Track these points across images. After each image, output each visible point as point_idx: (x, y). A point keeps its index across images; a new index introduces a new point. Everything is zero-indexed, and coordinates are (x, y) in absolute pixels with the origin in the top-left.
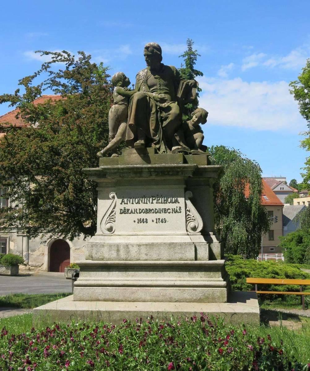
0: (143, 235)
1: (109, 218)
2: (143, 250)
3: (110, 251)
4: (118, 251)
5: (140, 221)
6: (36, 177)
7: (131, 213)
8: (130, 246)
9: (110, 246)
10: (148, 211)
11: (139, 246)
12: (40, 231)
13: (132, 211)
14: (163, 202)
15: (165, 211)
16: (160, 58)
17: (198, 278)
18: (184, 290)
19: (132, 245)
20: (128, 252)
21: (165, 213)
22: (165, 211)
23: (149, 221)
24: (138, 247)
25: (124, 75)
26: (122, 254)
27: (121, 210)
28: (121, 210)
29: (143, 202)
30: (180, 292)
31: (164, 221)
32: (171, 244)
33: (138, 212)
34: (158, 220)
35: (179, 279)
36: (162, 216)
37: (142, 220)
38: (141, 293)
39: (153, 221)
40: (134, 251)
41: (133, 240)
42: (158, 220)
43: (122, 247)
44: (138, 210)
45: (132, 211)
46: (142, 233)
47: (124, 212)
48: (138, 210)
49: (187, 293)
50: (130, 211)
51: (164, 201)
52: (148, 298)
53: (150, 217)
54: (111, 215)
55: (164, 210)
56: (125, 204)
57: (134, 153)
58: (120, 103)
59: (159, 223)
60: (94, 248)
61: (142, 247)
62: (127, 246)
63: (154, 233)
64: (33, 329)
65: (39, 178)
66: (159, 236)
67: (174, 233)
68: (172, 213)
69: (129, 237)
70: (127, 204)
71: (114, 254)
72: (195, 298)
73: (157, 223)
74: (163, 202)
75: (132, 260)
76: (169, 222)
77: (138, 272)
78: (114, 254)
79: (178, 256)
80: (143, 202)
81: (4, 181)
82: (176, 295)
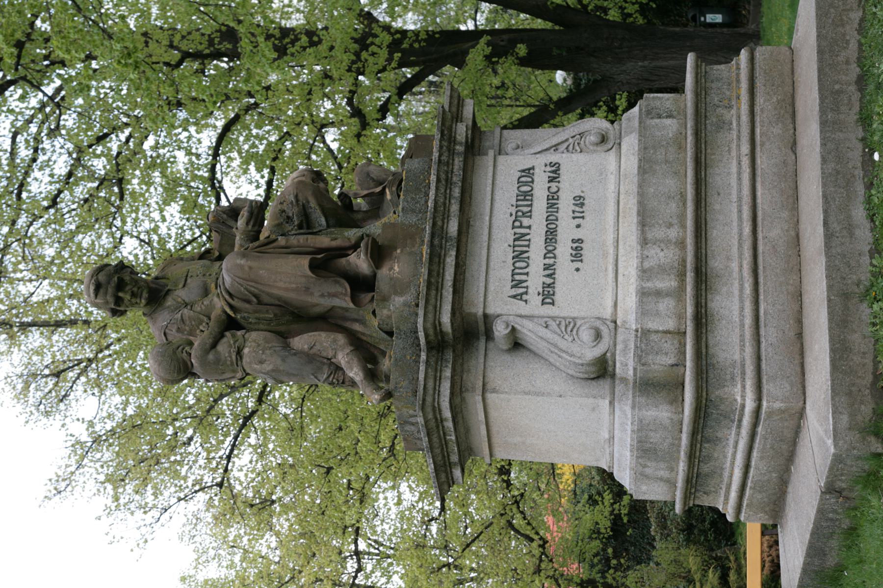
2: (657, 233)
4: (658, 294)
5: (577, 255)
7: (554, 279)
8: (646, 265)
10: (551, 236)
12: (381, 548)
14: (529, 203)
15: (553, 200)
19: (643, 259)
21: (557, 199)
22: (553, 200)
23: (578, 233)
26: (668, 283)
30: (767, 144)
31: (579, 201)
33: (551, 261)
35: (734, 146)
36: (566, 205)
39: (578, 226)
42: (579, 215)
43: (649, 285)
44: (547, 261)
46: (611, 250)
48: (547, 261)
51: (527, 200)
56: (526, 293)
59: (583, 212)
61: (649, 236)
62: (645, 273)
66: (621, 211)
67: (613, 177)
68: (559, 182)
69: (620, 278)
70: (527, 287)
71: (666, 305)
73: (583, 217)
74: (529, 203)
75: (684, 261)
76: (584, 189)
78: (666, 305)
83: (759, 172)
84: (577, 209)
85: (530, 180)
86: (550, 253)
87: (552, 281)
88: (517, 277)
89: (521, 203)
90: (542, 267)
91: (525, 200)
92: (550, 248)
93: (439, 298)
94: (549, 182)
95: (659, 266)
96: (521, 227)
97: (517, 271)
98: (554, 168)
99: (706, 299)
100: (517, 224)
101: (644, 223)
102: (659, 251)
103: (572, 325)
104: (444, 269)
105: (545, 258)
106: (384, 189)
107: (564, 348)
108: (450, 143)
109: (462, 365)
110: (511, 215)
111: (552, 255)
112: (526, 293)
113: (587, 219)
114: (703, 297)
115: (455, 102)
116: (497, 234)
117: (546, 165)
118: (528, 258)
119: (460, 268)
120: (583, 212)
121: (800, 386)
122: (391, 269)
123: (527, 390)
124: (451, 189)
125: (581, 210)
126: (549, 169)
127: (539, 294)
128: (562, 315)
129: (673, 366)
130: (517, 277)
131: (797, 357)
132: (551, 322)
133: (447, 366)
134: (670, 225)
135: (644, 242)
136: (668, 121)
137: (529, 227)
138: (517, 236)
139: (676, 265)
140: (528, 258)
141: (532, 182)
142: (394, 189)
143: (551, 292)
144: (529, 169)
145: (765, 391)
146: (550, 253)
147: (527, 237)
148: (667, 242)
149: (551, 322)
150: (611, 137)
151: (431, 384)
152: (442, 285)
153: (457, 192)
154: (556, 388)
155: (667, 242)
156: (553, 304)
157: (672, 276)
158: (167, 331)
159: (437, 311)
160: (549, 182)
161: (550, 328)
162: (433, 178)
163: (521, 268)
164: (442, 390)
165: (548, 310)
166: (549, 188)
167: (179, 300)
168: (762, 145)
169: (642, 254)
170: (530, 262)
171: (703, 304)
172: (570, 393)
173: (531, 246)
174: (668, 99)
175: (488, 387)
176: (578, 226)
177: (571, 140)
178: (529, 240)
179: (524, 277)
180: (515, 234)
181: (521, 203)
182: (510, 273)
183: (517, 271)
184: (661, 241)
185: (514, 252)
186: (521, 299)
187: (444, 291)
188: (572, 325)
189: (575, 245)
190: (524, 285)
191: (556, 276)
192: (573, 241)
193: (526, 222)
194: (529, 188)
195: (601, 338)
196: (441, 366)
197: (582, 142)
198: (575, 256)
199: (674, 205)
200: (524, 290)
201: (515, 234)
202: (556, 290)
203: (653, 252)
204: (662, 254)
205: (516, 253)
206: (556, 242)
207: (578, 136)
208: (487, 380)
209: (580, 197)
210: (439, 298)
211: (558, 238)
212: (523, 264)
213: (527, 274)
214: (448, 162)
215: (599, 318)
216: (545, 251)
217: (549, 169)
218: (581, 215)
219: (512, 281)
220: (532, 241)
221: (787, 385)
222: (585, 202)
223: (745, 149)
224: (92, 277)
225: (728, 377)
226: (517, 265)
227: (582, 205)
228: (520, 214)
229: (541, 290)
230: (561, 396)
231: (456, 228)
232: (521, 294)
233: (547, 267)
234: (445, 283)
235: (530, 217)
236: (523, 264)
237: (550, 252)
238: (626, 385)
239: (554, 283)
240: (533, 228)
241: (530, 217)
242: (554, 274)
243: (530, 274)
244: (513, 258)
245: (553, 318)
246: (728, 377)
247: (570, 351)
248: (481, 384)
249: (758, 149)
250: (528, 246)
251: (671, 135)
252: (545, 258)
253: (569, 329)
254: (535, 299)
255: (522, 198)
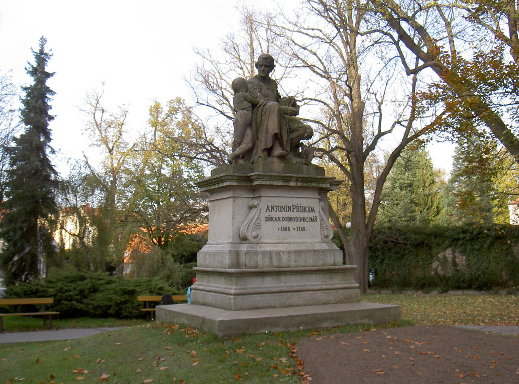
0: (287, 243)
1: (254, 226)
2: (293, 257)
3: (264, 258)
4: (271, 258)
5: (284, 229)
8: (281, 254)
9: (264, 253)
10: (290, 219)
11: (289, 253)
15: (304, 219)
17: (337, 282)
18: (329, 293)
20: (279, 259)
22: (304, 219)
26: (275, 262)
27: (266, 217)
28: (266, 217)
31: (303, 229)
32: (315, 251)
34: (298, 228)
38: (295, 298)
39: (294, 229)
40: (285, 258)
41: (281, 248)
43: (274, 255)
47: (269, 219)
49: (331, 296)
50: (274, 219)
52: (301, 302)
53: (292, 225)
54: (256, 223)
57: (276, 162)
58: (248, 109)
60: (247, 256)
61: (292, 254)
62: (278, 253)
63: (296, 241)
64: (484, 366)
69: (276, 245)
71: (267, 262)
72: (337, 299)
75: (283, 267)
79: (321, 262)
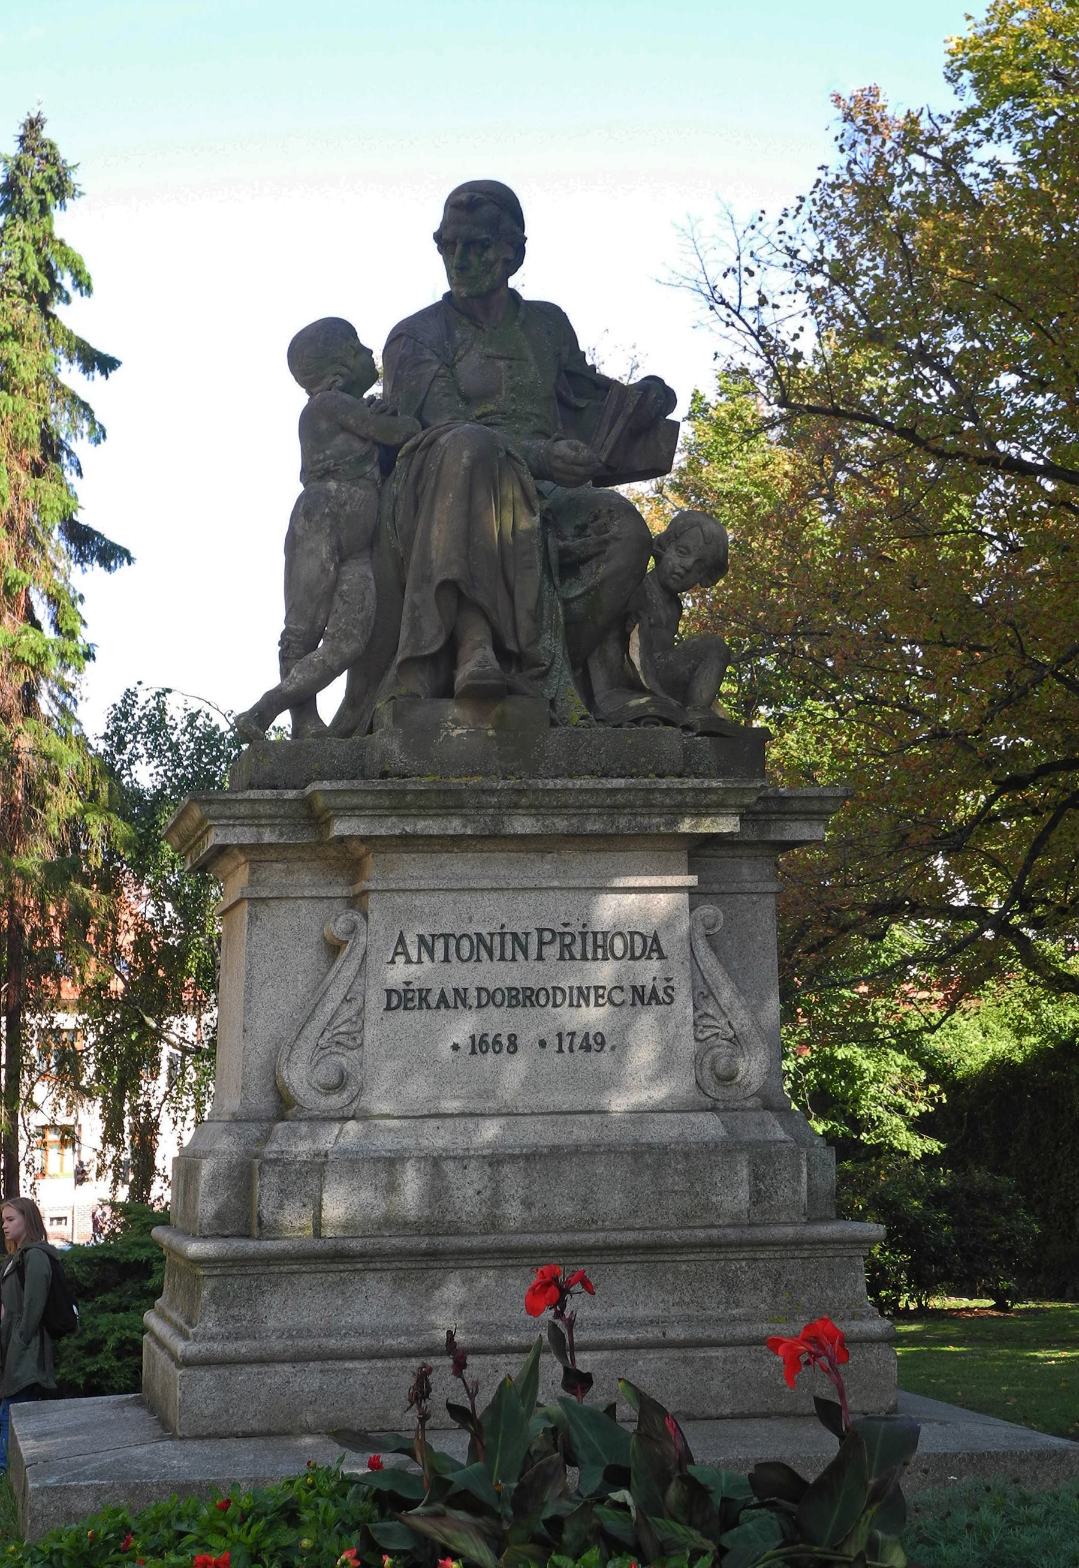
2: (513, 1180)
6: (972, 424)
8: (449, 1166)
13: (443, 994)
16: (516, 255)
24: (489, 1170)
25: (109, 569)
29: (497, 953)
30: (689, 1371)
37: (490, 1040)
39: (543, 1044)
45: (443, 994)
50: (433, 999)
51: (595, 952)
55: (592, 992)
56: (409, 961)
59: (571, 1050)
61: (507, 1169)
65: (907, 491)
68: (633, 1005)
75: (458, 1233)
77: (827, 1427)
80: (497, 953)
81: (497, 397)
82: (671, 1387)
83: (630, 1355)
84: (578, 1041)
85: (637, 954)
86: (488, 998)
87: (434, 1005)
88: (440, 945)
89: (590, 940)
90: (461, 986)
91: (596, 946)
92: (499, 997)
93: (378, 812)
94: (634, 988)
95: (447, 1188)
96: (541, 943)
97: (452, 942)
98: (661, 994)
99: (382, 1270)
100: (548, 937)
101: (531, 1157)
102: (476, 1187)
103: (351, 1044)
104: (438, 815)
105: (479, 989)
106: (650, 693)
107: (305, 1033)
108: (694, 806)
109: (300, 859)
110: (566, 925)
111: (484, 1002)
112: (409, 961)
113: (558, 1058)
114: (385, 1266)
115: (816, 806)
116: (525, 904)
117: (668, 980)
118: (478, 960)
119: (455, 843)
120: (571, 1050)
121: (211, 1430)
122: (457, 723)
123: (255, 972)
124: (600, 815)
125: (576, 1047)
126: (660, 986)
127: (408, 983)
128: (367, 1025)
129: (259, 1218)
130: (440, 945)
131: (264, 1426)
132: (356, 1005)
133: (281, 834)
134: (527, 1204)
135: (495, 1160)
136: (743, 1193)
137: (540, 958)
138: (523, 938)
139: (448, 1218)
140: (478, 960)
141: (633, 958)
142: (651, 710)
143: (410, 1005)
144: (659, 950)
145: (200, 1373)
146: (488, 998)
147: (520, 956)
148: (496, 1199)
149: (356, 1005)
150: (731, 1093)
151: (243, 810)
152: (407, 816)
153: (593, 826)
154: (259, 1022)
155: (496, 1199)
156: (389, 1008)
157: (427, 1212)
158: (404, 339)
159: (353, 811)
160: (634, 988)
161: (346, 1006)
162: (620, 783)
163: (458, 950)
164: (238, 830)
165: (375, 1000)
166: (621, 988)
167: (461, 352)
168: (686, 1361)
169: (470, 1157)
170: (471, 965)
171: (372, 1266)
172: (250, 1046)
173: (502, 964)
174: (795, 1192)
175: (261, 908)
176: (543, 1044)
177: (723, 1022)
178: (514, 959)
179: (439, 954)
180: (527, 934)
181: (590, 940)
182: (447, 931)
183: (452, 942)
184: (496, 1191)
185: (492, 935)
186: (396, 954)
187: (394, 819)
188: (351, 1044)
189: (505, 1042)
190: (425, 957)
191: (443, 1010)
192: (513, 1039)
193: (552, 951)
194: (619, 953)
195: (326, 1095)
196: (282, 826)
197: (719, 1042)
198: (483, 1041)
199: (569, 1210)
200: (415, 958)
201: (527, 934)
202: (416, 1013)
203: (475, 1176)
204: (470, 1192)
205: (488, 939)
206: (510, 1006)
207: (731, 1033)
208: (273, 903)
209: (603, 1044)
210: (378, 812)
211: (519, 1010)
212: (465, 952)
213: (446, 960)
214: (653, 806)
215: (361, 1089)
216: (491, 989)
217: (660, 986)
218: (565, 1047)
219: (433, 936)
220: (511, 965)
221: (211, 1409)
222: (593, 1054)
223: (677, 1333)
224: (488, 193)
225: (235, 1311)
226: (465, 944)
227: (587, 1048)
228: (568, 940)
229: (415, 986)
230: (245, 1031)
231: (520, 830)
232: (406, 953)
233: (461, 995)
234: (411, 820)
235: (562, 958)
236: (465, 952)
237: (491, 997)
238: (258, 1140)
239: (429, 1007)
240: (539, 965)
241: (562, 958)
242: (447, 1007)
243: (447, 966)
244: (478, 935)
245: (360, 1012)
246: (235, 1311)
247: (300, 1042)
248: (263, 895)
249: (677, 1353)
250: (502, 958)
251: (714, 1199)
252: (479, 989)
253: (340, 1038)
254: (398, 974)
255: (600, 942)
